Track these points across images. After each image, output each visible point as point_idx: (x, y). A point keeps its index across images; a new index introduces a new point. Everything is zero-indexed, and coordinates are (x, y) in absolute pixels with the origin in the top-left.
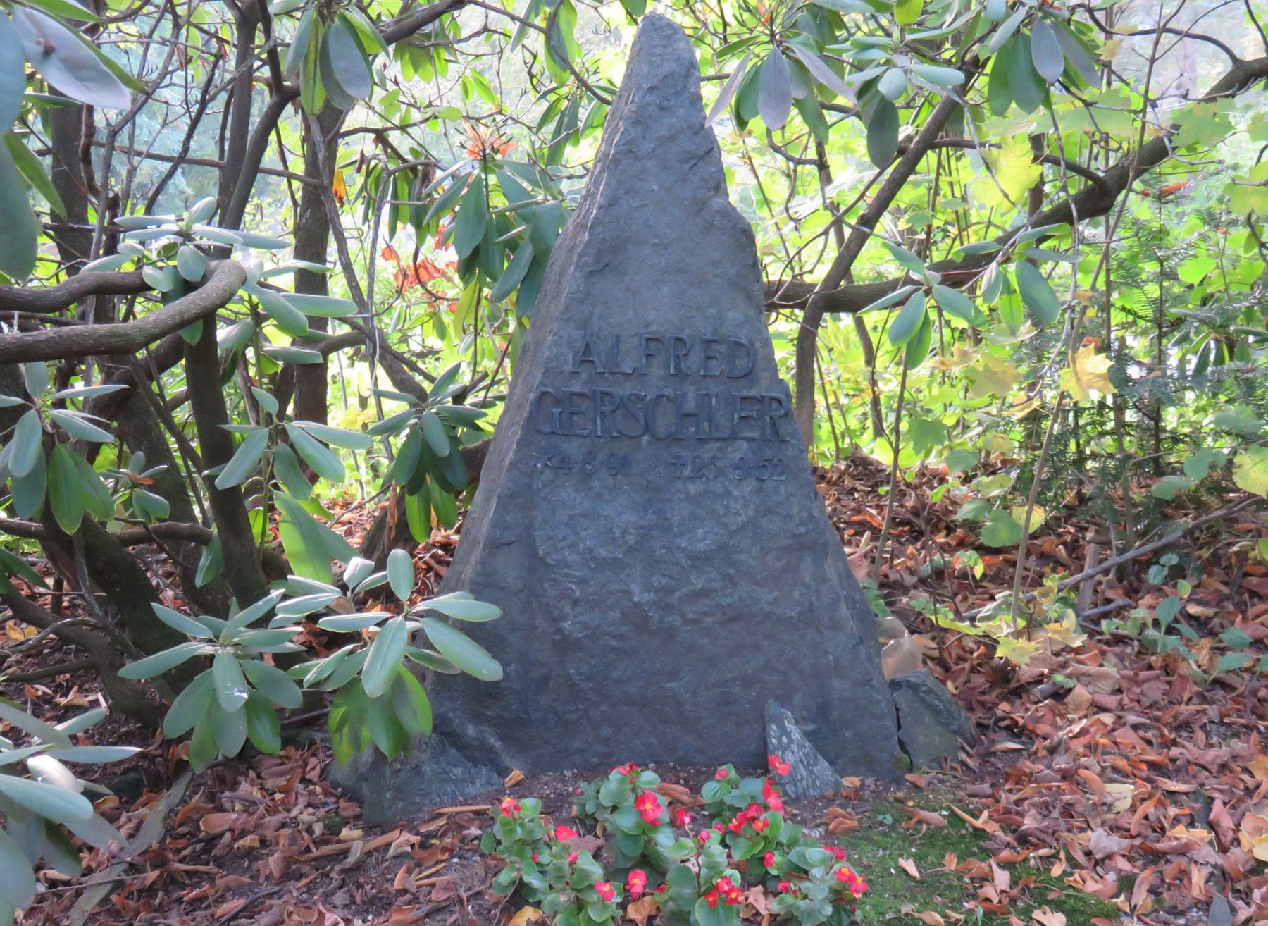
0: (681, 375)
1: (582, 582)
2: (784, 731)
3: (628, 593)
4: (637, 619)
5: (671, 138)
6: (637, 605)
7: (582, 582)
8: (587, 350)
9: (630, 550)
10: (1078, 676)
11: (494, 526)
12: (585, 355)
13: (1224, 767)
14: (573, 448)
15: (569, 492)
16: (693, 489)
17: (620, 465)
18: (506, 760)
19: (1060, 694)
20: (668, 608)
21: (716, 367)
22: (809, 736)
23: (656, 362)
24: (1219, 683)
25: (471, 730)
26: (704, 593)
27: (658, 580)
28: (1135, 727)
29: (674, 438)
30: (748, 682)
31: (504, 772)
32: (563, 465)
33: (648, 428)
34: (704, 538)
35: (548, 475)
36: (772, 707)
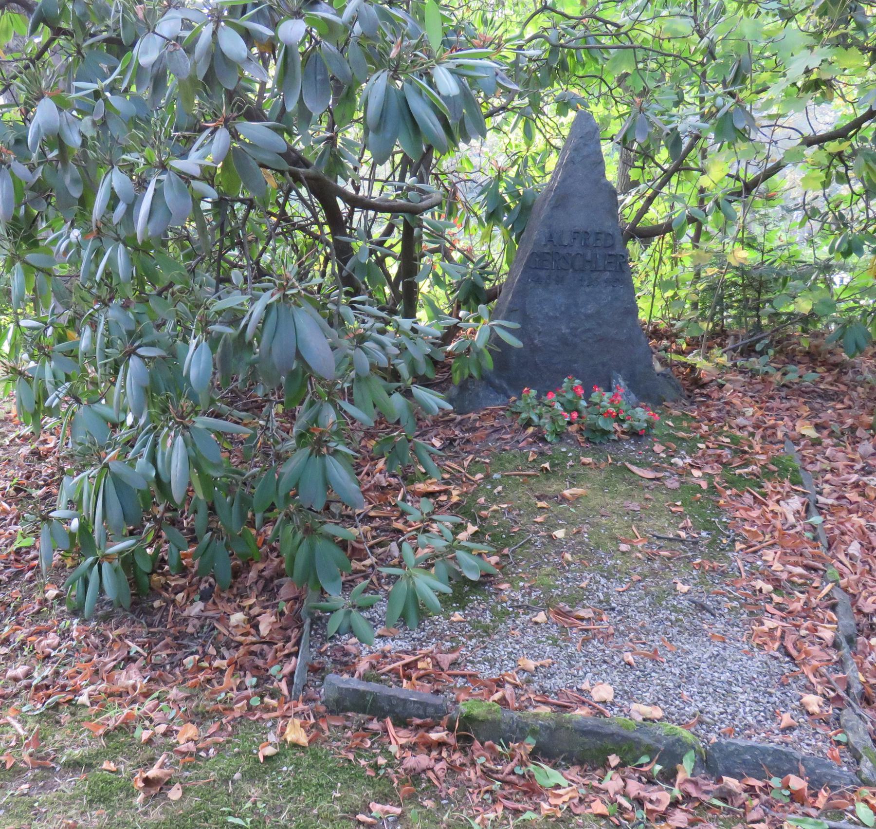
0: (586, 246)
1: (542, 325)
2: (618, 382)
3: (560, 329)
4: (564, 340)
5: (588, 156)
6: (564, 334)
7: (542, 325)
8: (551, 236)
9: (562, 313)
10: (728, 381)
11: (511, 303)
12: (550, 239)
13: (788, 409)
14: (543, 274)
15: (540, 290)
16: (588, 290)
17: (560, 281)
18: (509, 393)
19: (721, 386)
20: (575, 336)
21: (599, 243)
22: (628, 386)
23: (577, 241)
24: (784, 385)
25: (497, 381)
26: (589, 330)
27: (572, 325)
28: (752, 397)
29: (582, 270)
30: (604, 365)
31: (509, 397)
32: (538, 281)
33: (572, 266)
34: (591, 309)
35: (532, 284)
36: (615, 373)
